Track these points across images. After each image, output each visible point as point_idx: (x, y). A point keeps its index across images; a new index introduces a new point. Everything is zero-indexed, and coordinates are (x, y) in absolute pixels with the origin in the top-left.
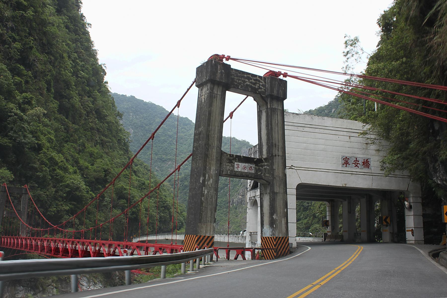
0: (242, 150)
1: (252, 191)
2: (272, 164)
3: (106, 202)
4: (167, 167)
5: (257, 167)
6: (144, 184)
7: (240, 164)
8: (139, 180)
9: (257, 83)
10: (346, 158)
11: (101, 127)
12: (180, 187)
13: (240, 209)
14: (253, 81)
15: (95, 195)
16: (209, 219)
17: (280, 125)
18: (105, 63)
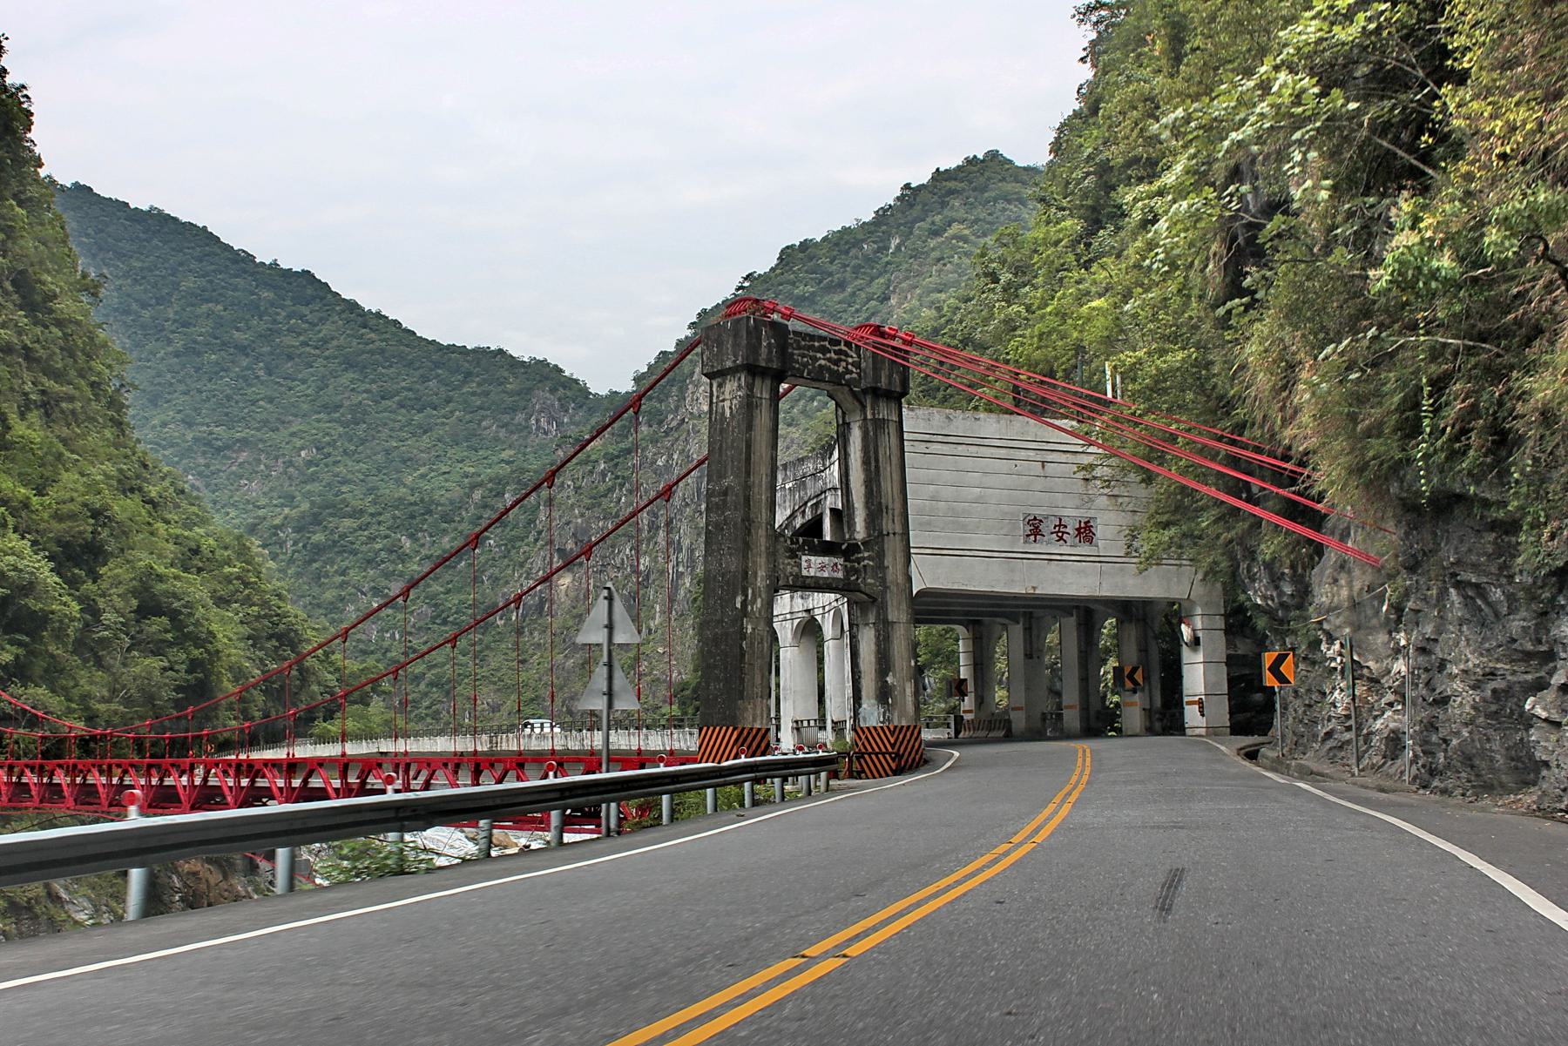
0: (534, 401)
2: (881, 555)
3: (108, 628)
4: (233, 473)
5: (848, 564)
6: (196, 551)
7: (813, 558)
8: (177, 537)
9: (841, 360)
10: (1035, 519)
11: (38, 341)
12: (294, 551)
13: (536, 634)
14: (833, 355)
16: (758, 690)
17: (895, 460)
18: (22, 82)
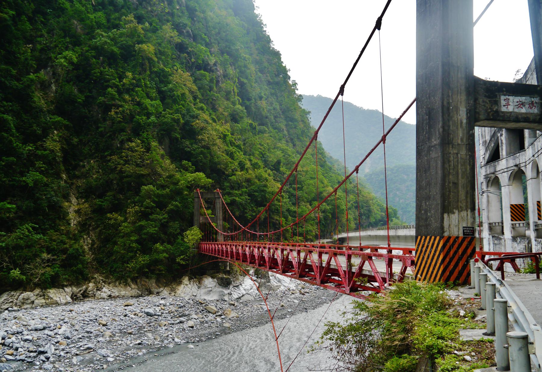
1: (488, 166)
7: (511, 98)
15: (320, 356)
16: (178, 46)
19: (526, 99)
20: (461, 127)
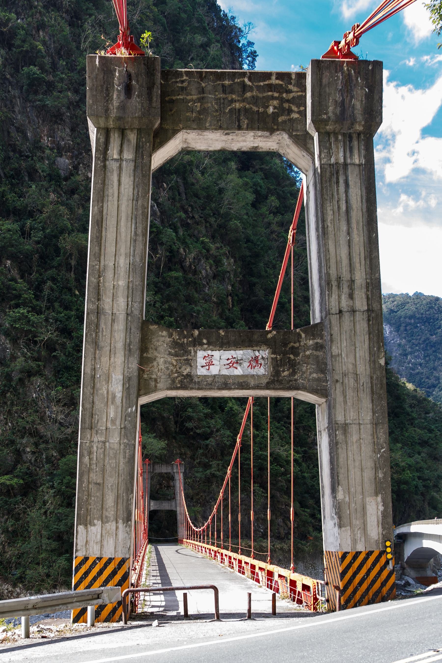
7: (216, 354)
19: (244, 354)
20: (112, 403)
